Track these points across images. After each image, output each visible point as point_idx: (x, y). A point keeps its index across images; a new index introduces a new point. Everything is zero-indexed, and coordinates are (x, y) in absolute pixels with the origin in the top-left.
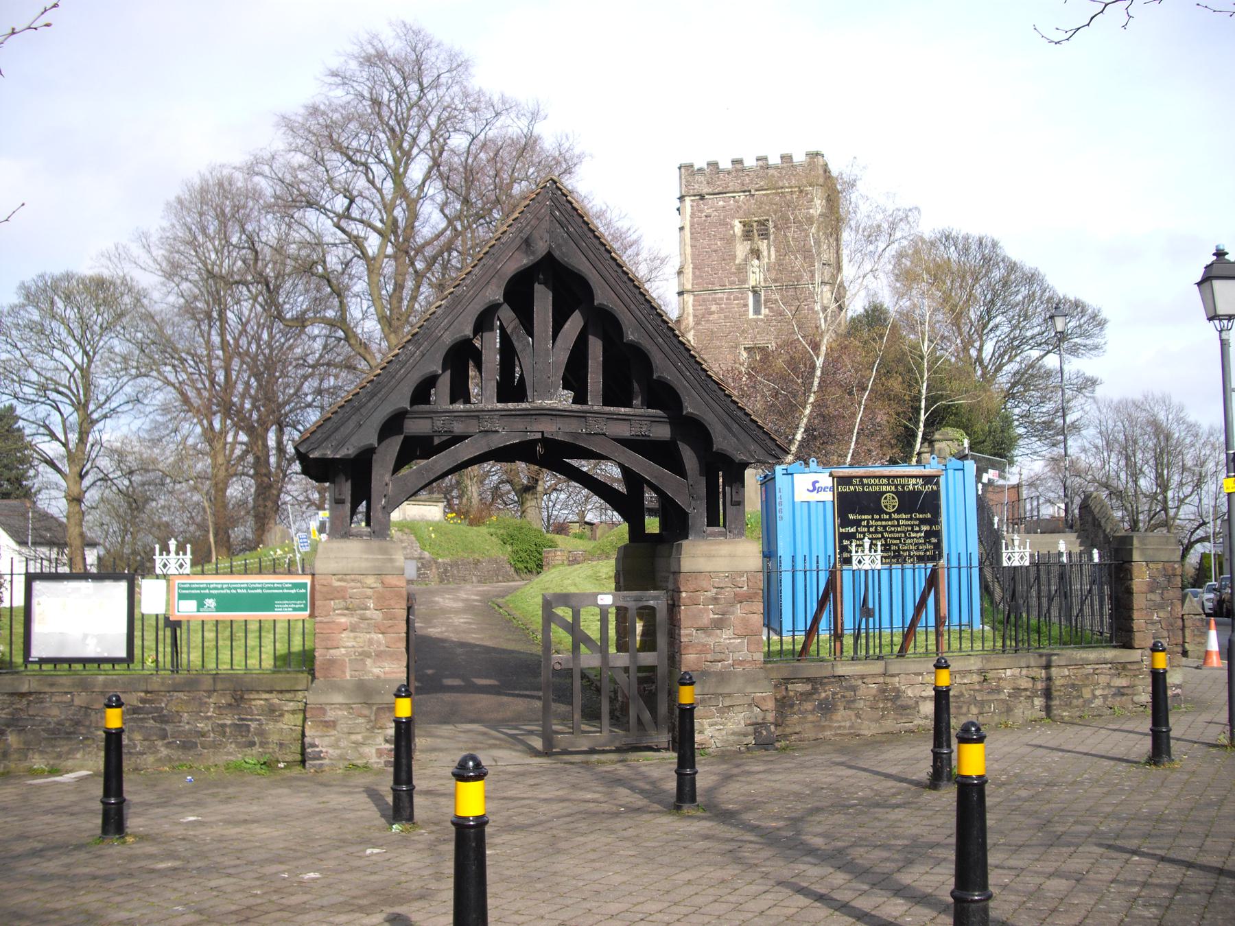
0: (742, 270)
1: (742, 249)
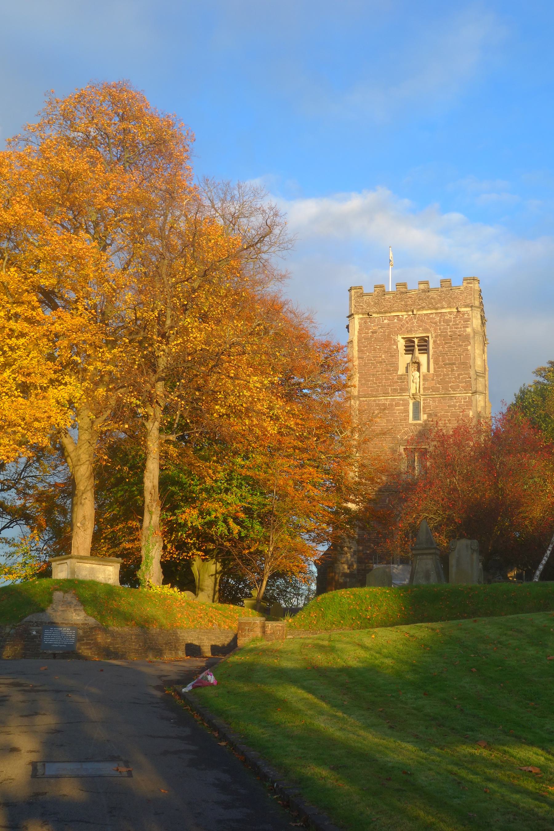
0: (404, 379)
1: (404, 359)
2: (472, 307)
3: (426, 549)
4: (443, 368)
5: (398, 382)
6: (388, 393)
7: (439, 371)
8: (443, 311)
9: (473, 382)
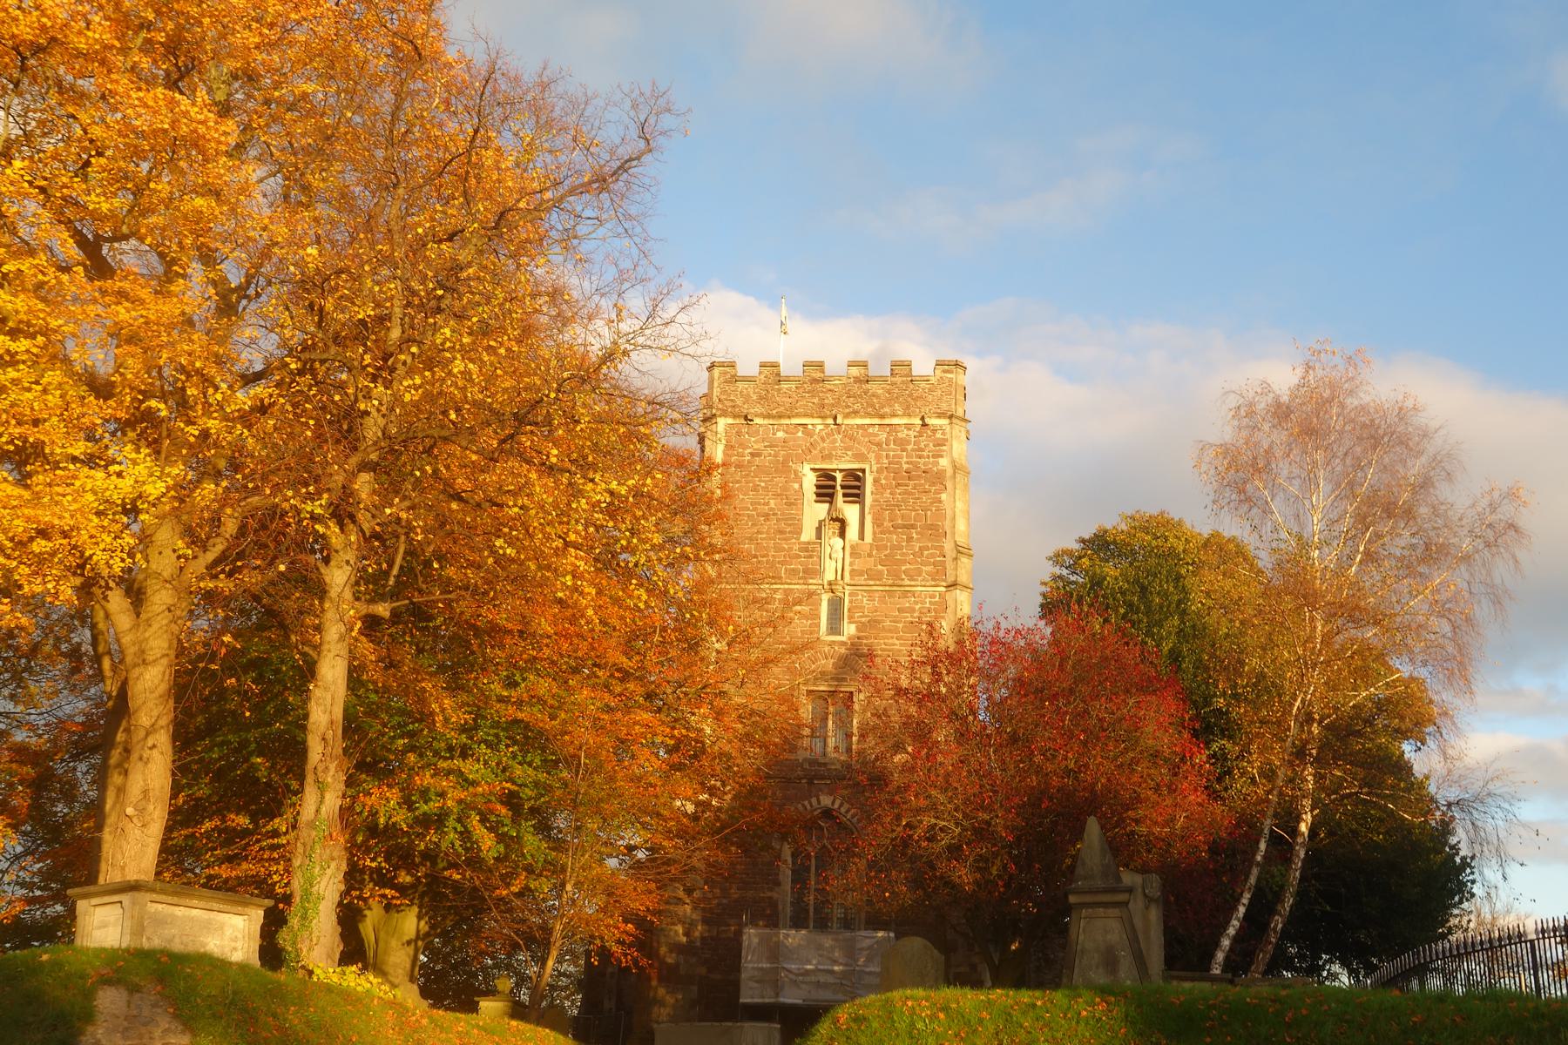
0: (812, 550)
1: (815, 512)
2: (951, 417)
3: (1106, 891)
4: (890, 533)
5: (800, 556)
6: (780, 578)
7: (882, 540)
8: (895, 421)
9: (949, 565)
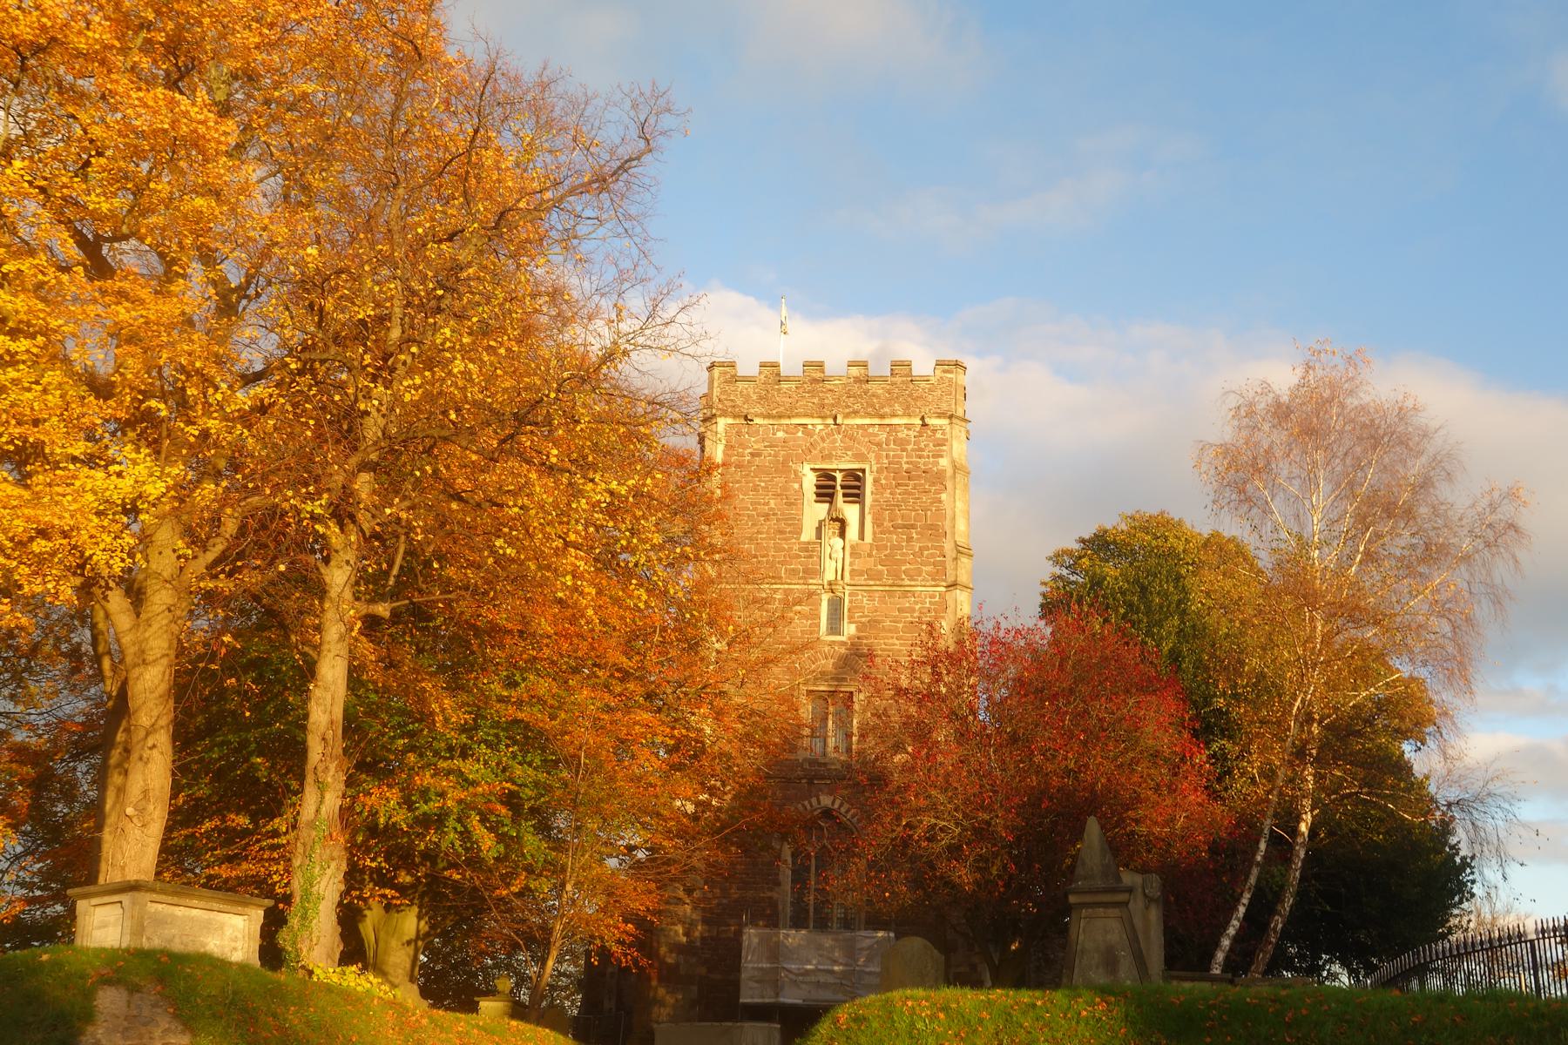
0: (812, 550)
1: (815, 512)
2: (951, 417)
3: (1106, 891)
4: (890, 533)
5: (800, 556)
6: (780, 578)
7: (882, 540)
8: (895, 421)
9: (949, 565)
